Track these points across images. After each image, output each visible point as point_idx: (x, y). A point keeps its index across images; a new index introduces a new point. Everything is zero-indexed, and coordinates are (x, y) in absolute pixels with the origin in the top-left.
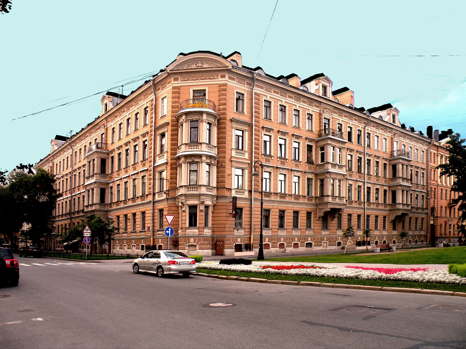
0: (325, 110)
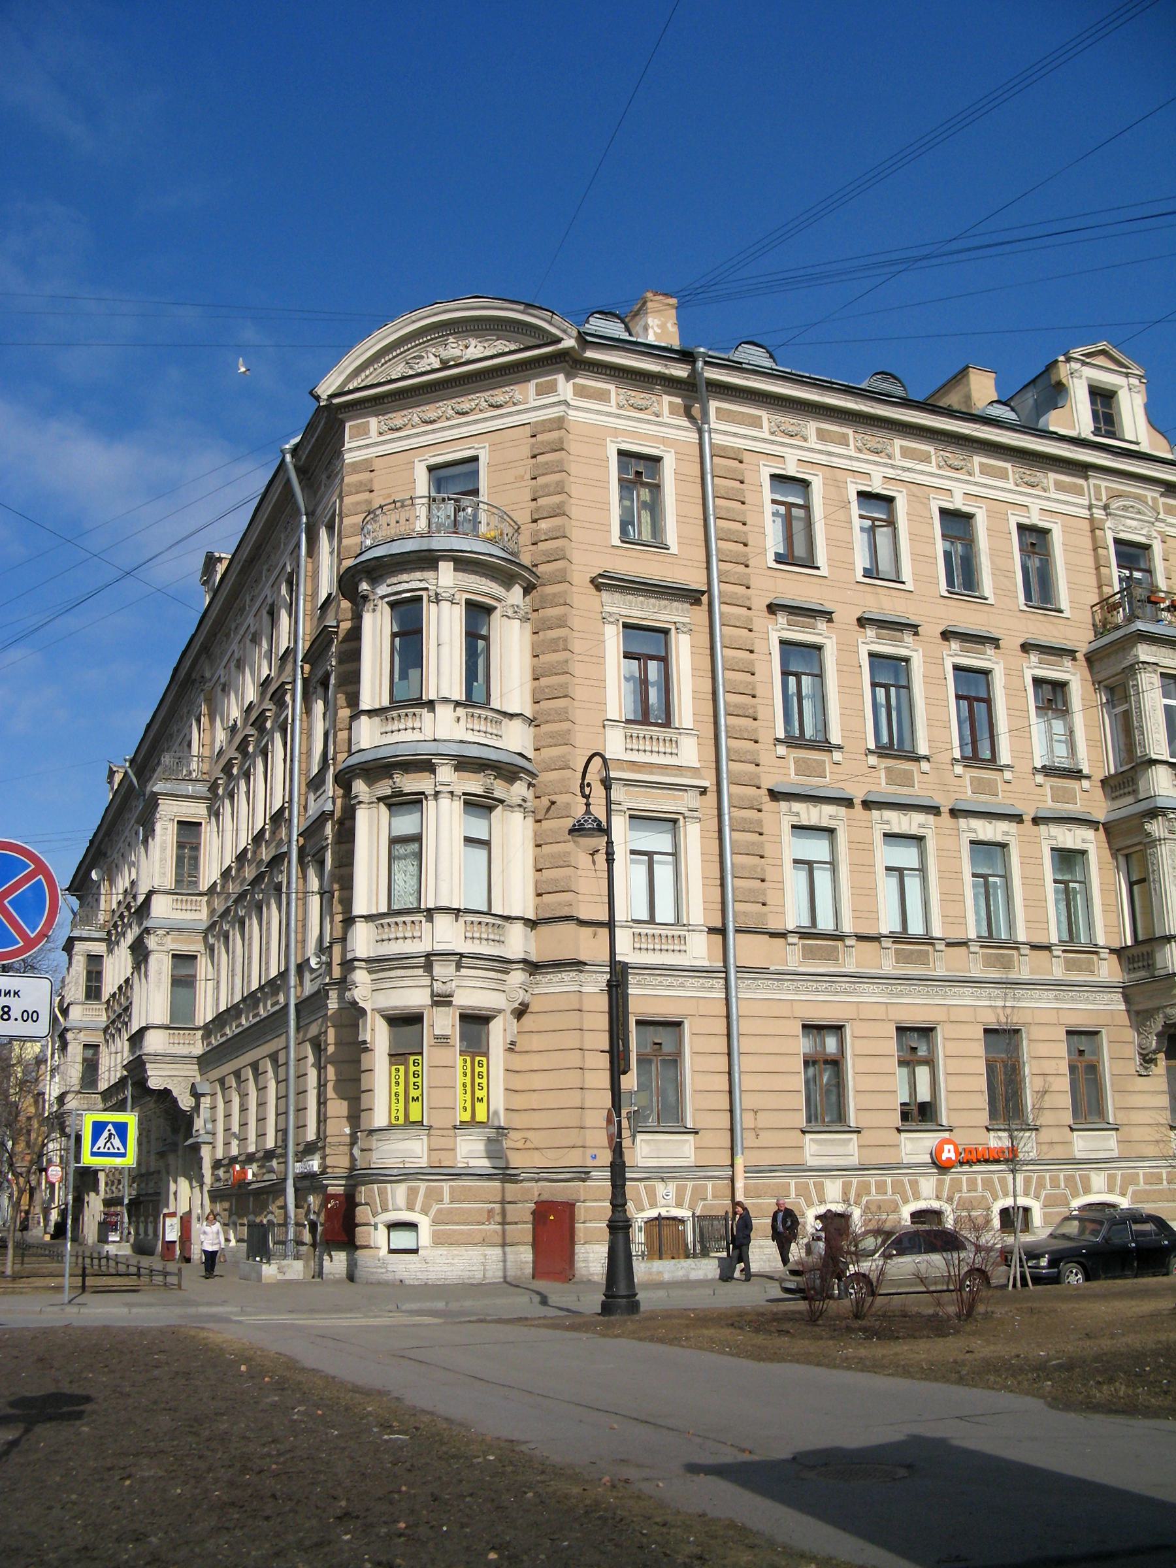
0: (1115, 504)
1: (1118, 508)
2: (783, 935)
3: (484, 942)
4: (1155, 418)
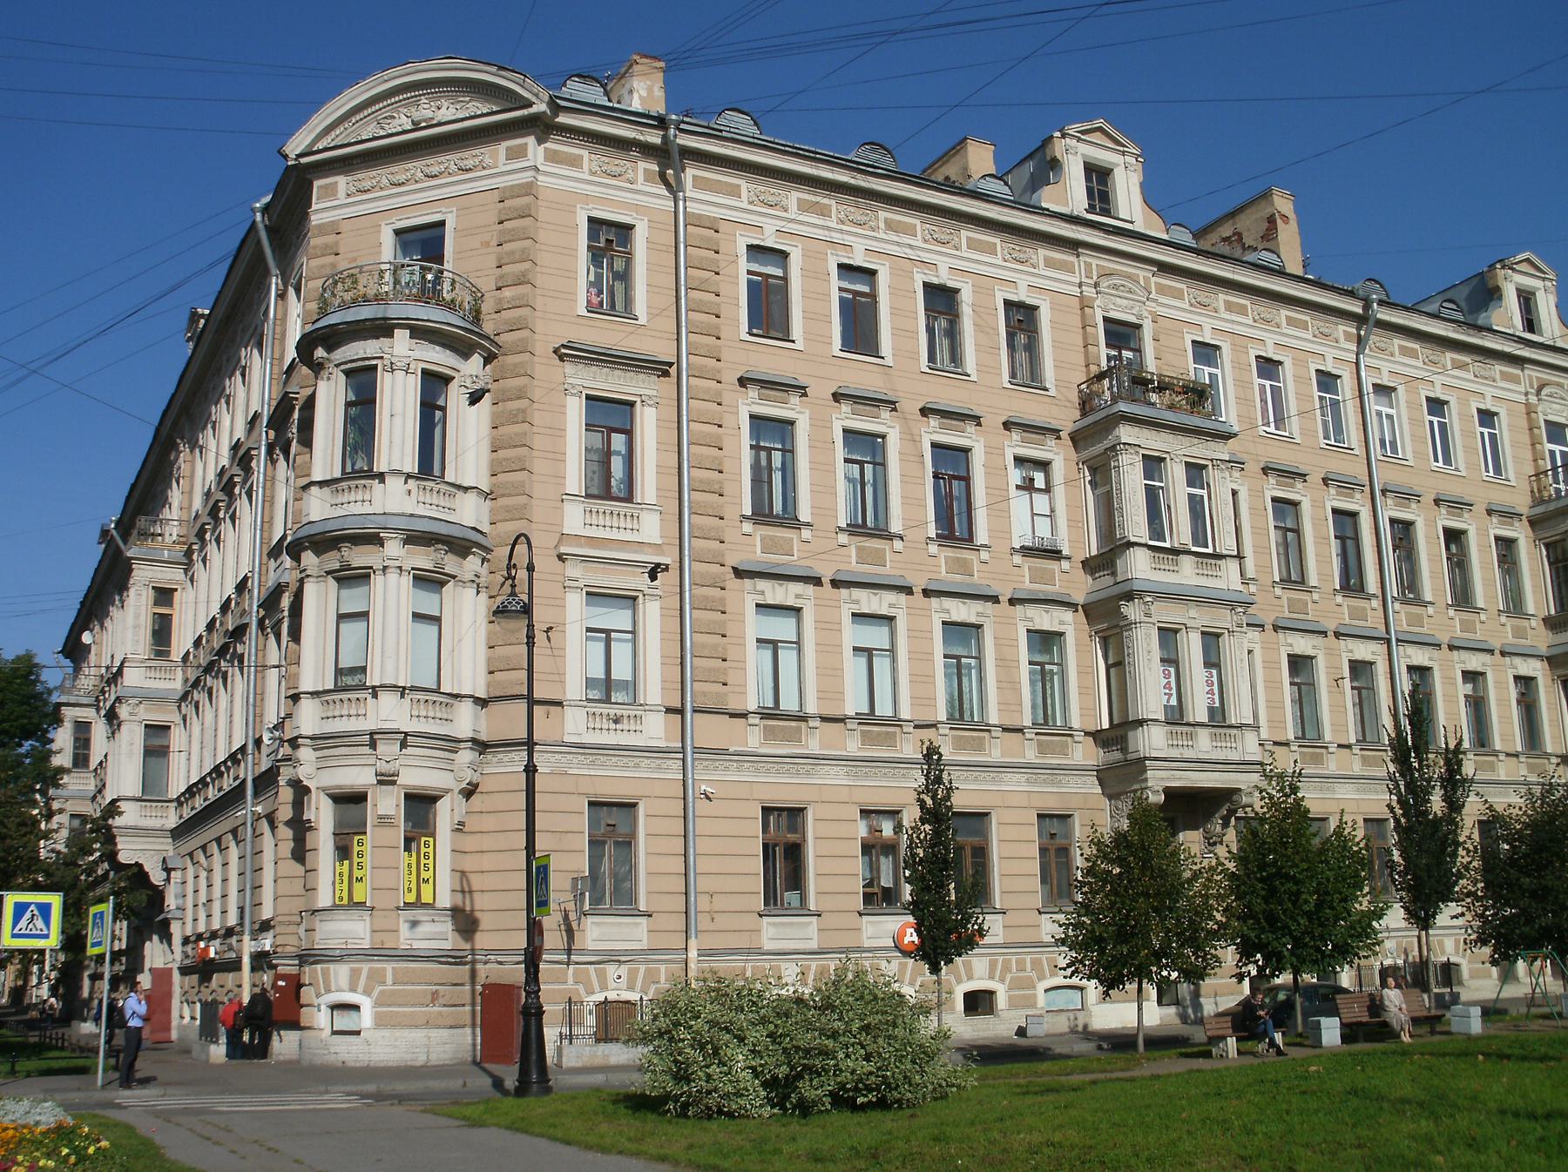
0: (1104, 283)
1: (1109, 287)
2: (744, 716)
3: (431, 720)
4: (1151, 197)
